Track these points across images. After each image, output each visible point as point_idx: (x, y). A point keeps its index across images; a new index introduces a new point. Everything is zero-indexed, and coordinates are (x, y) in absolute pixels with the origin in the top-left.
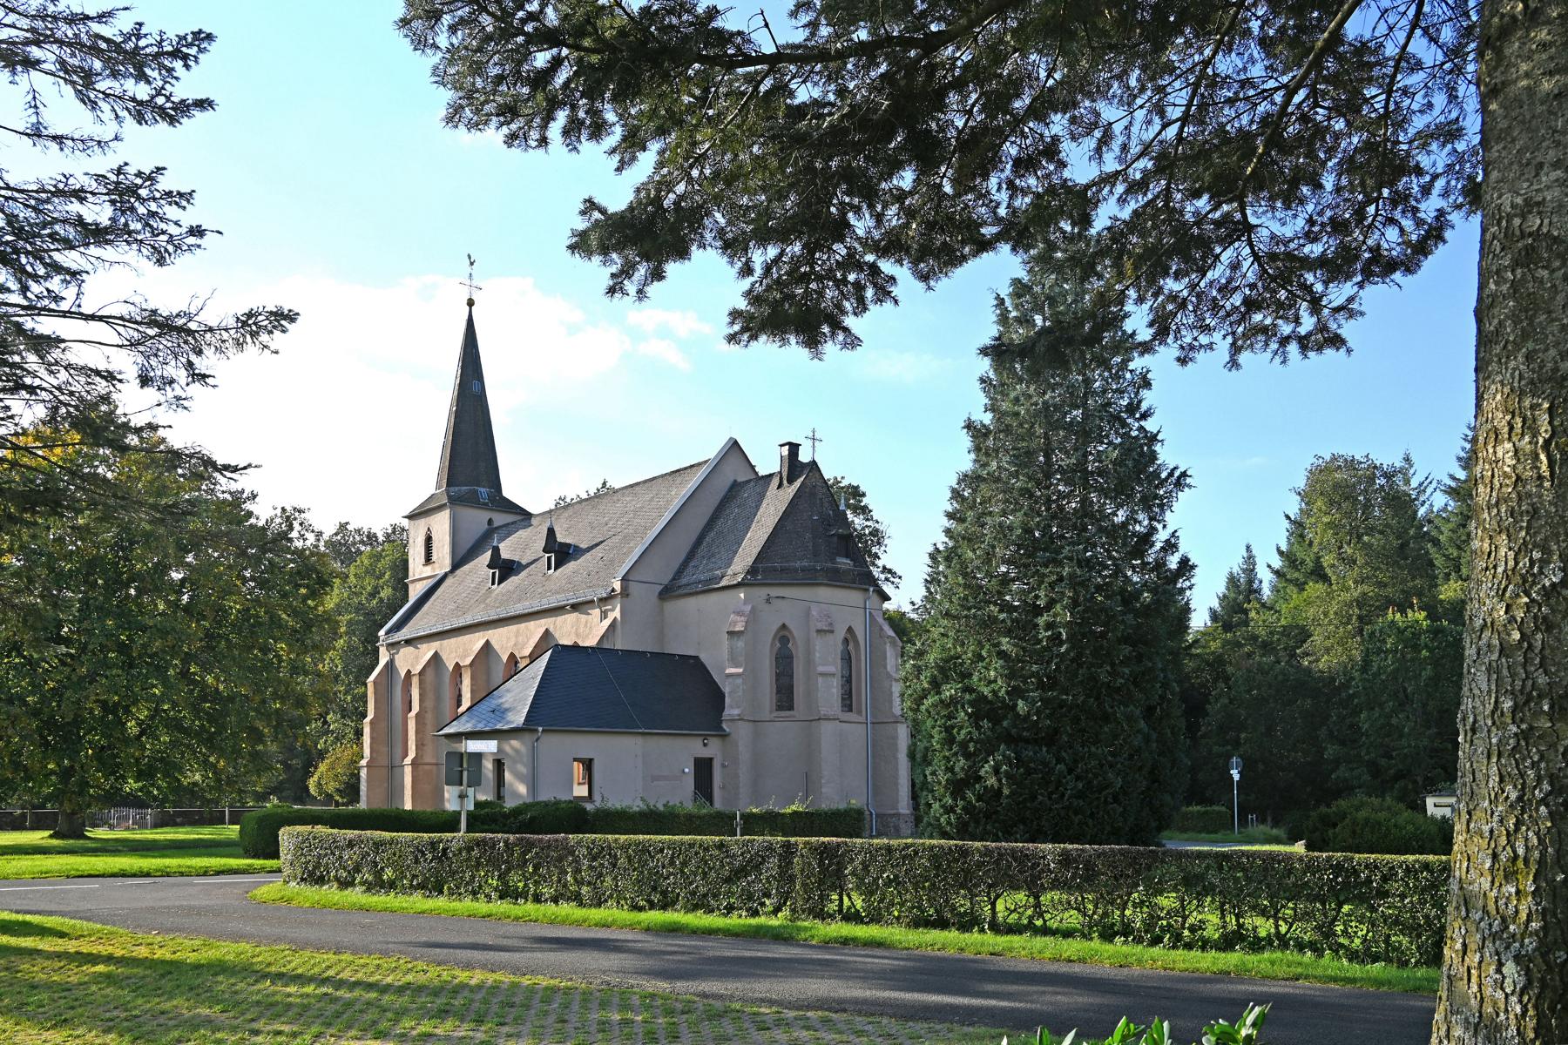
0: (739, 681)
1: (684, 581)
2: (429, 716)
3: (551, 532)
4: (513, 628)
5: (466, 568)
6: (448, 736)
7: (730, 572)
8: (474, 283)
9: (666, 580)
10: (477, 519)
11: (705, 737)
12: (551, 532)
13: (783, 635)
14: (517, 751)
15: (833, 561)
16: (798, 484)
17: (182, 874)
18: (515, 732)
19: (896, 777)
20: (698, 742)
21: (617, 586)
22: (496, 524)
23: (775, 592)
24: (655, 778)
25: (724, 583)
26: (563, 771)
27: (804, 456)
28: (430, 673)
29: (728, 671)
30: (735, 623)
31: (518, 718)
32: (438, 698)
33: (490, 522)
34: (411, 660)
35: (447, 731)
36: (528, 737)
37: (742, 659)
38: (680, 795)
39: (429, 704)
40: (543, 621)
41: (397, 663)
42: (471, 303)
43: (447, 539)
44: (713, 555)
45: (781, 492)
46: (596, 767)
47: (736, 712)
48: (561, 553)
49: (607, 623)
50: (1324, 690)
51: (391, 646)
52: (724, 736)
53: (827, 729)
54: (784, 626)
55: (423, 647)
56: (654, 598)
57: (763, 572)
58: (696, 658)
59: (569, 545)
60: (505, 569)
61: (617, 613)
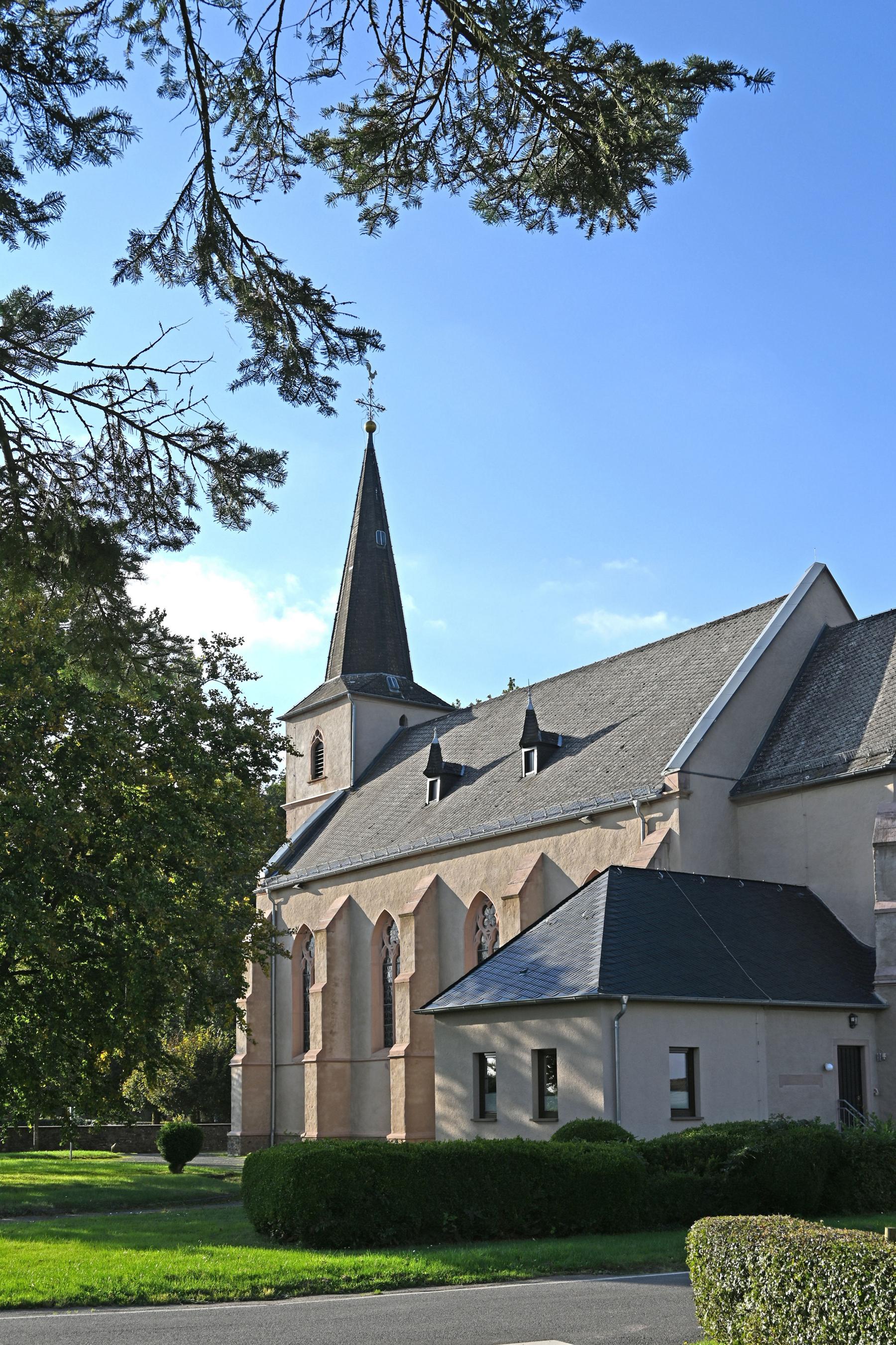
1: (772, 773)
2: (340, 991)
3: (531, 715)
6: (438, 1014)
7: (862, 751)
10: (387, 716)
11: (852, 1013)
12: (531, 715)
18: (586, 1003)
19: (387, 1090)
20: (842, 1020)
21: (673, 782)
22: (411, 723)
24: (786, 1080)
25: (853, 770)
26: (609, 1078)
28: (341, 926)
29: (878, 906)
31: (589, 979)
32: (354, 966)
33: (403, 720)
35: (438, 1005)
36: (606, 1012)
39: (341, 972)
40: (535, 843)
42: (371, 428)
43: (347, 744)
44: (816, 732)
48: (548, 748)
49: (656, 838)
52: (878, 1010)
55: (328, 891)
56: (725, 802)
58: (804, 889)
59: (555, 736)
60: (449, 777)
61: (673, 823)
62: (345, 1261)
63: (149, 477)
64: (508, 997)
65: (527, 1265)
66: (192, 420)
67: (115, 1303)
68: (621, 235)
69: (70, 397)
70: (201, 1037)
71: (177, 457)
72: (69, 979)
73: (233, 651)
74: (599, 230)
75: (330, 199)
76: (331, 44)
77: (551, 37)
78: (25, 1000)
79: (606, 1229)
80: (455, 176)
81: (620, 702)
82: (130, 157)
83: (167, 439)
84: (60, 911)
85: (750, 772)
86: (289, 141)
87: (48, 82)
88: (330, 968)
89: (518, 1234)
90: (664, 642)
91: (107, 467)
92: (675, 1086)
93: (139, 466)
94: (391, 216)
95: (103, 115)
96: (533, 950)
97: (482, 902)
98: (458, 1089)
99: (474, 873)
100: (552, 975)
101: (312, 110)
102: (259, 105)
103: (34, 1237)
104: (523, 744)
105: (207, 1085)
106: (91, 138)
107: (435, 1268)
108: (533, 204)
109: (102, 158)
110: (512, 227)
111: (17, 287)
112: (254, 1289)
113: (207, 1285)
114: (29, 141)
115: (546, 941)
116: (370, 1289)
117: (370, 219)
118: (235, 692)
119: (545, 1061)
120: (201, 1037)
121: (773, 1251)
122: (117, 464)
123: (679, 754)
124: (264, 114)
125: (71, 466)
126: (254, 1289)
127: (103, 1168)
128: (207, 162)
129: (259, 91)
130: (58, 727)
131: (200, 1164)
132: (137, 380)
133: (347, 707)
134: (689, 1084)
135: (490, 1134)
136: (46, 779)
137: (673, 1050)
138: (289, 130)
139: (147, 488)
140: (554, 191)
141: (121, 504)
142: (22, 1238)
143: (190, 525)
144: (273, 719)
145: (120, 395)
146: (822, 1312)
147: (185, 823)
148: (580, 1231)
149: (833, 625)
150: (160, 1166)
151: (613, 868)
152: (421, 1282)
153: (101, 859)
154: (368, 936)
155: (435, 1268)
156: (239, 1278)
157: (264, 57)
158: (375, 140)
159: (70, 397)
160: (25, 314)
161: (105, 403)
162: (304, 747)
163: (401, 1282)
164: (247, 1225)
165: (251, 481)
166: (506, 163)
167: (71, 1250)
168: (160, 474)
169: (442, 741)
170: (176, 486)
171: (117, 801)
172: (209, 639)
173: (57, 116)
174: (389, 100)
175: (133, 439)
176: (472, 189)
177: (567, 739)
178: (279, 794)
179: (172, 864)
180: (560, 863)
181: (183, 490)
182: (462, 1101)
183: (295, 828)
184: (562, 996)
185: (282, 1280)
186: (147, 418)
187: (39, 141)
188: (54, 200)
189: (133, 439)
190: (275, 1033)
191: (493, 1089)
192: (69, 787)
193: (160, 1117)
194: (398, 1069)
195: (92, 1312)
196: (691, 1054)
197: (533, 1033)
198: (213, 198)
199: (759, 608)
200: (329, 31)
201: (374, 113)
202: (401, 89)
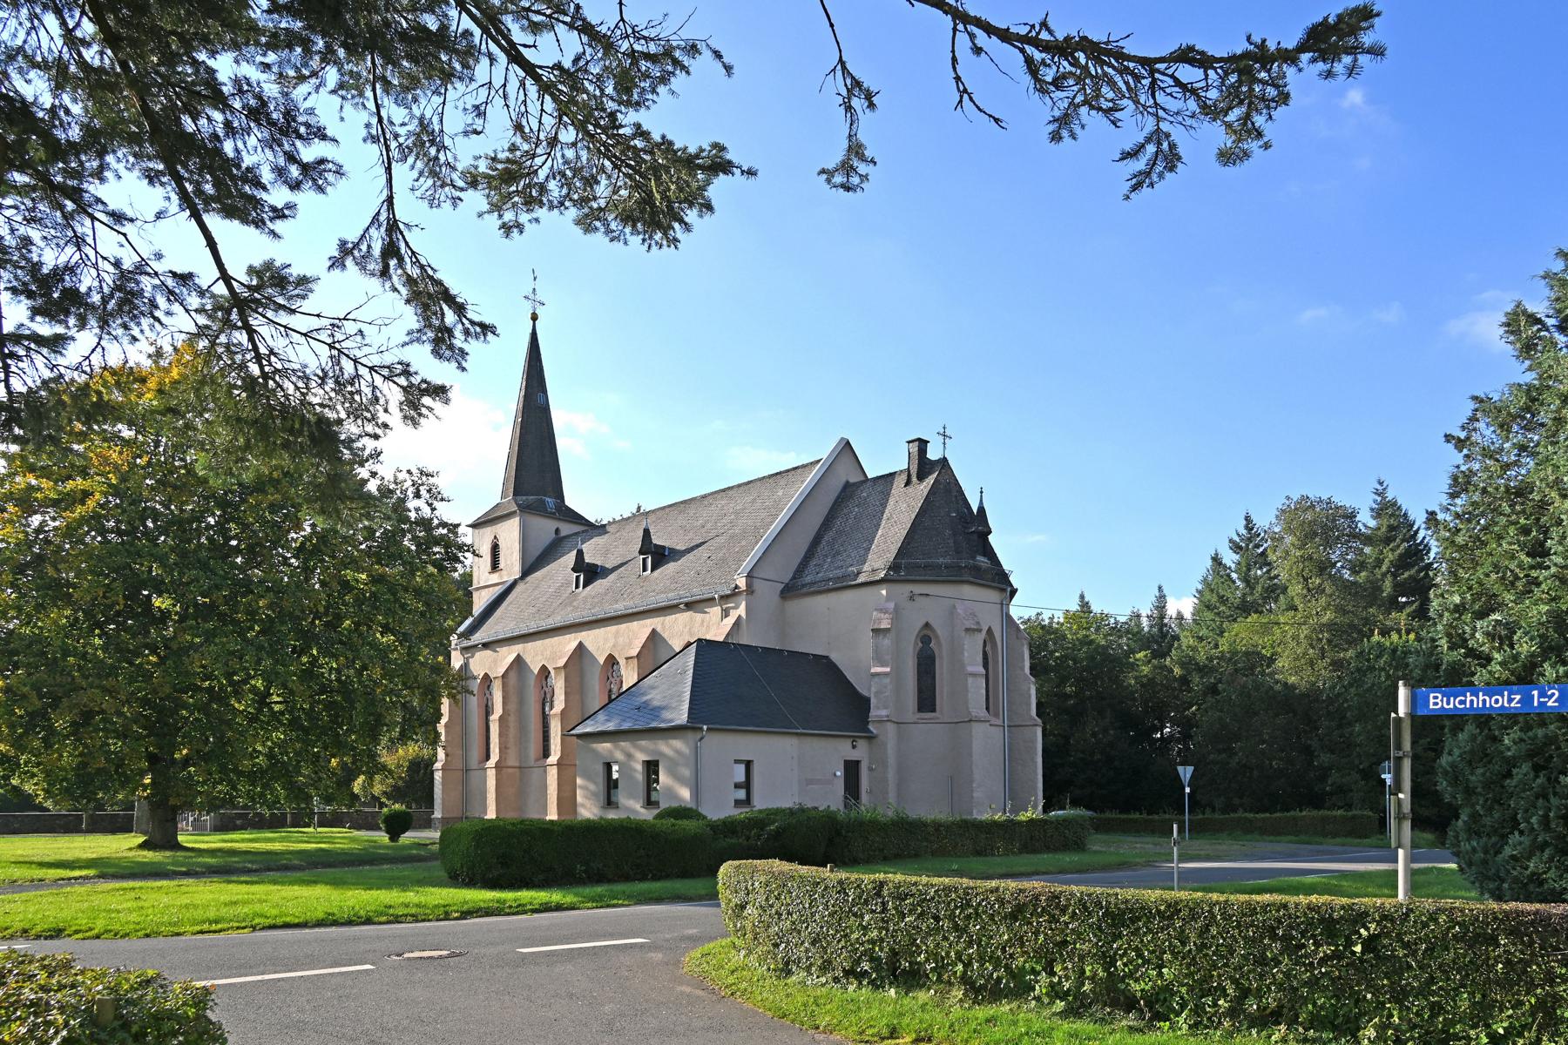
0: (887, 681)
1: (808, 579)
3: (647, 532)
4: (612, 629)
5: (538, 574)
6: (579, 736)
7: (866, 567)
8: (538, 298)
9: (787, 578)
10: (546, 528)
11: (854, 739)
12: (647, 532)
13: (926, 636)
14: (678, 752)
15: (974, 558)
16: (931, 480)
17: (416, 919)
21: (742, 583)
23: (918, 589)
24: (810, 782)
26: (696, 779)
27: (933, 454)
28: (513, 676)
29: (873, 670)
30: (880, 620)
31: (680, 714)
32: (522, 702)
33: (557, 531)
34: (481, 664)
36: (691, 736)
37: (888, 658)
38: (831, 799)
39: (512, 707)
40: (648, 621)
41: (472, 666)
42: (534, 318)
43: (516, 547)
44: (838, 553)
45: (910, 489)
46: (756, 769)
47: (884, 712)
48: (658, 556)
49: (730, 621)
50: (1291, 703)
51: (465, 649)
52: (871, 738)
53: (978, 730)
54: (927, 625)
55: (503, 650)
56: (776, 598)
57: (905, 567)
59: (663, 547)
60: (590, 573)
61: (742, 611)
62: (508, 896)
63: (359, 392)
64: (626, 726)
65: (629, 897)
66: (388, 359)
67: (350, 923)
68: (668, 251)
69: (305, 335)
70: (411, 750)
71: (378, 380)
72: (312, 708)
73: (431, 480)
74: (654, 248)
75: (480, 215)
76: (478, 115)
77: (621, 126)
78: (280, 722)
79: (685, 874)
80: (562, 204)
81: (709, 526)
82: (339, 190)
83: (371, 369)
84: (305, 659)
85: (794, 578)
86: (455, 176)
87: (287, 135)
88: (504, 703)
89: (626, 878)
90: (739, 486)
91: (330, 384)
92: (737, 786)
93: (352, 385)
94: (520, 227)
95: (322, 161)
96: (644, 694)
97: (612, 661)
98: (592, 787)
99: (606, 640)
100: (656, 711)
101: (465, 153)
102: (433, 151)
103: (292, 883)
104: (641, 553)
105: (418, 781)
106: (315, 174)
107: (569, 899)
108: (613, 226)
109: (321, 190)
110: (599, 238)
111: (267, 258)
112: (446, 913)
113: (413, 911)
114: (273, 170)
115: (653, 688)
116: (525, 912)
117: (507, 229)
118: (433, 509)
119: (652, 767)
120: (411, 750)
121: (762, 879)
122: (337, 382)
123: (747, 563)
124: (437, 158)
125: (306, 378)
126: (446, 913)
127: (342, 838)
128: (390, 200)
129: (432, 142)
130: (298, 527)
131: (408, 837)
132: (350, 327)
133: (517, 520)
134: (747, 785)
135: (612, 815)
136: (291, 565)
137: (737, 762)
138: (454, 169)
139: (357, 398)
140: (628, 218)
141: (339, 407)
142: (283, 883)
143: (386, 426)
144: (461, 530)
145: (339, 336)
146: (789, 913)
147: (397, 600)
148: (667, 877)
149: (852, 481)
150: (382, 837)
151: (699, 640)
152: (559, 908)
153: (333, 625)
154: (532, 682)
155: (569, 899)
156: (436, 906)
157: (435, 120)
158: (509, 176)
159: (305, 335)
160: (272, 277)
161: (329, 341)
162: (485, 550)
163: (546, 908)
164: (443, 874)
165: (426, 400)
166: (595, 199)
167: (320, 891)
168: (367, 391)
169: (585, 547)
170: (377, 399)
171: (346, 586)
172: (415, 471)
173: (291, 158)
174: (518, 153)
175: (348, 367)
176: (573, 212)
177: (672, 551)
178: (467, 579)
179: (386, 630)
180: (665, 636)
181: (382, 401)
182: (595, 794)
183: (480, 602)
184: (663, 725)
185: (465, 908)
186: (358, 354)
187: (280, 172)
188: (291, 206)
189: (348, 367)
190: (465, 747)
191: (616, 787)
192: (308, 571)
193: (382, 805)
194: (552, 774)
195: (333, 929)
196: (748, 764)
197: (642, 750)
198: (393, 227)
199: (804, 466)
200: (477, 107)
201: (508, 161)
202: (526, 147)
